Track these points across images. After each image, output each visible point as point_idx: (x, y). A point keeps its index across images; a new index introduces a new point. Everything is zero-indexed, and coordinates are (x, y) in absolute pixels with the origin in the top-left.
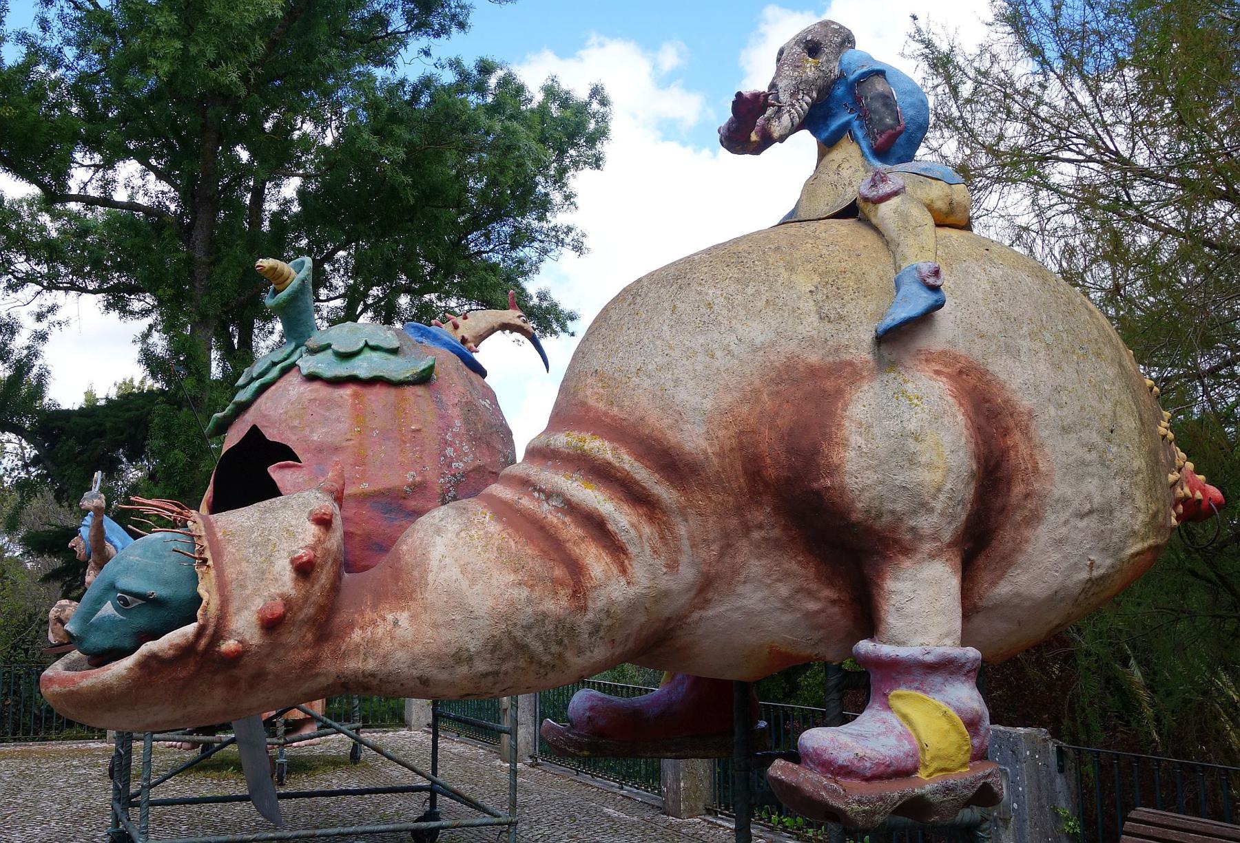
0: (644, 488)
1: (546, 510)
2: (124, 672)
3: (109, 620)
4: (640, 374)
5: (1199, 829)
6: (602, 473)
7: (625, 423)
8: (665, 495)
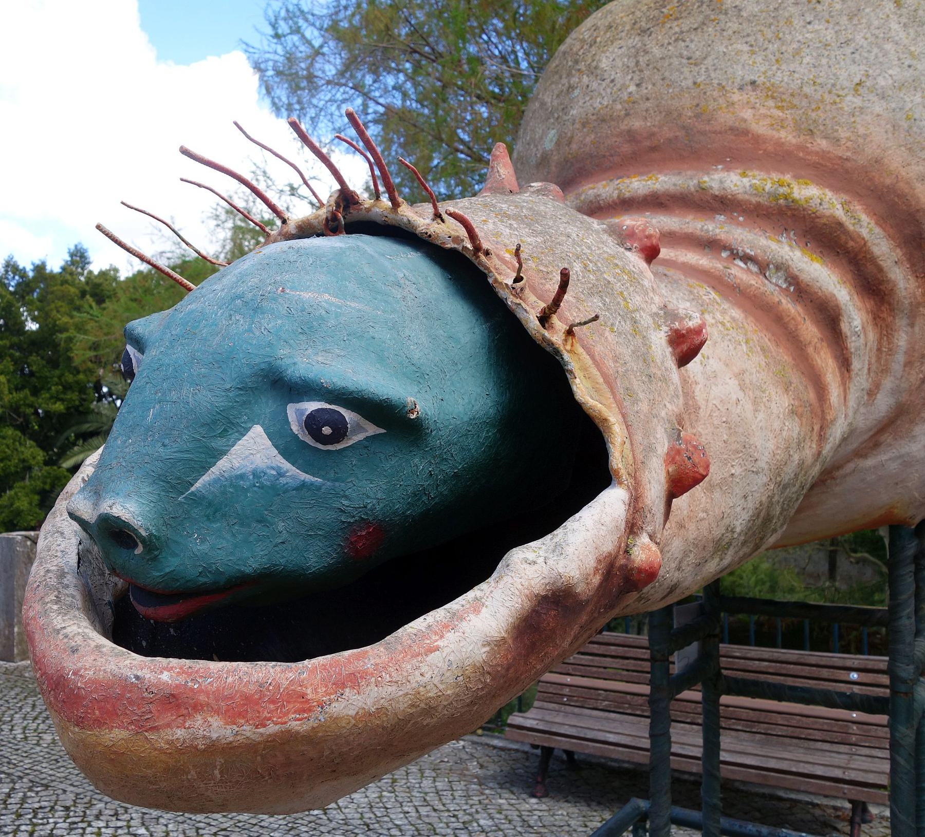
0: (880, 269)
1: (772, 288)
2: (481, 654)
3: (267, 488)
4: (861, 91)
5: (617, 642)
6: (827, 238)
7: (848, 165)
8: (901, 284)
